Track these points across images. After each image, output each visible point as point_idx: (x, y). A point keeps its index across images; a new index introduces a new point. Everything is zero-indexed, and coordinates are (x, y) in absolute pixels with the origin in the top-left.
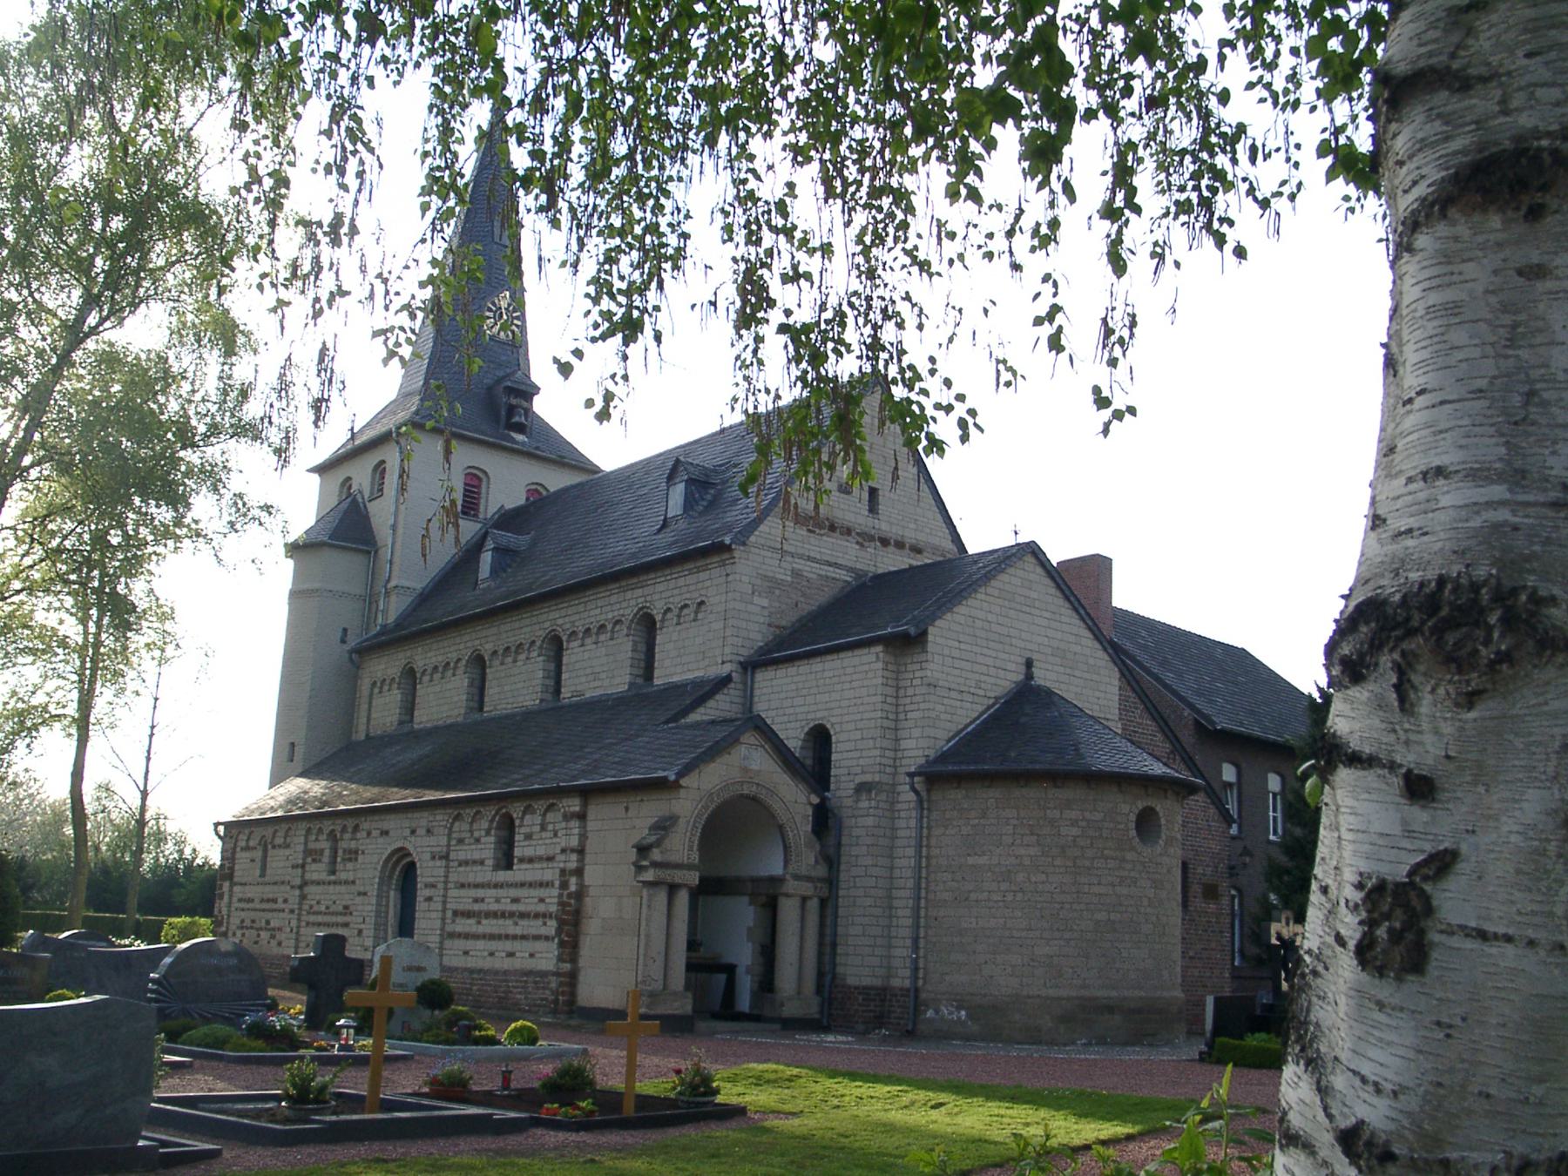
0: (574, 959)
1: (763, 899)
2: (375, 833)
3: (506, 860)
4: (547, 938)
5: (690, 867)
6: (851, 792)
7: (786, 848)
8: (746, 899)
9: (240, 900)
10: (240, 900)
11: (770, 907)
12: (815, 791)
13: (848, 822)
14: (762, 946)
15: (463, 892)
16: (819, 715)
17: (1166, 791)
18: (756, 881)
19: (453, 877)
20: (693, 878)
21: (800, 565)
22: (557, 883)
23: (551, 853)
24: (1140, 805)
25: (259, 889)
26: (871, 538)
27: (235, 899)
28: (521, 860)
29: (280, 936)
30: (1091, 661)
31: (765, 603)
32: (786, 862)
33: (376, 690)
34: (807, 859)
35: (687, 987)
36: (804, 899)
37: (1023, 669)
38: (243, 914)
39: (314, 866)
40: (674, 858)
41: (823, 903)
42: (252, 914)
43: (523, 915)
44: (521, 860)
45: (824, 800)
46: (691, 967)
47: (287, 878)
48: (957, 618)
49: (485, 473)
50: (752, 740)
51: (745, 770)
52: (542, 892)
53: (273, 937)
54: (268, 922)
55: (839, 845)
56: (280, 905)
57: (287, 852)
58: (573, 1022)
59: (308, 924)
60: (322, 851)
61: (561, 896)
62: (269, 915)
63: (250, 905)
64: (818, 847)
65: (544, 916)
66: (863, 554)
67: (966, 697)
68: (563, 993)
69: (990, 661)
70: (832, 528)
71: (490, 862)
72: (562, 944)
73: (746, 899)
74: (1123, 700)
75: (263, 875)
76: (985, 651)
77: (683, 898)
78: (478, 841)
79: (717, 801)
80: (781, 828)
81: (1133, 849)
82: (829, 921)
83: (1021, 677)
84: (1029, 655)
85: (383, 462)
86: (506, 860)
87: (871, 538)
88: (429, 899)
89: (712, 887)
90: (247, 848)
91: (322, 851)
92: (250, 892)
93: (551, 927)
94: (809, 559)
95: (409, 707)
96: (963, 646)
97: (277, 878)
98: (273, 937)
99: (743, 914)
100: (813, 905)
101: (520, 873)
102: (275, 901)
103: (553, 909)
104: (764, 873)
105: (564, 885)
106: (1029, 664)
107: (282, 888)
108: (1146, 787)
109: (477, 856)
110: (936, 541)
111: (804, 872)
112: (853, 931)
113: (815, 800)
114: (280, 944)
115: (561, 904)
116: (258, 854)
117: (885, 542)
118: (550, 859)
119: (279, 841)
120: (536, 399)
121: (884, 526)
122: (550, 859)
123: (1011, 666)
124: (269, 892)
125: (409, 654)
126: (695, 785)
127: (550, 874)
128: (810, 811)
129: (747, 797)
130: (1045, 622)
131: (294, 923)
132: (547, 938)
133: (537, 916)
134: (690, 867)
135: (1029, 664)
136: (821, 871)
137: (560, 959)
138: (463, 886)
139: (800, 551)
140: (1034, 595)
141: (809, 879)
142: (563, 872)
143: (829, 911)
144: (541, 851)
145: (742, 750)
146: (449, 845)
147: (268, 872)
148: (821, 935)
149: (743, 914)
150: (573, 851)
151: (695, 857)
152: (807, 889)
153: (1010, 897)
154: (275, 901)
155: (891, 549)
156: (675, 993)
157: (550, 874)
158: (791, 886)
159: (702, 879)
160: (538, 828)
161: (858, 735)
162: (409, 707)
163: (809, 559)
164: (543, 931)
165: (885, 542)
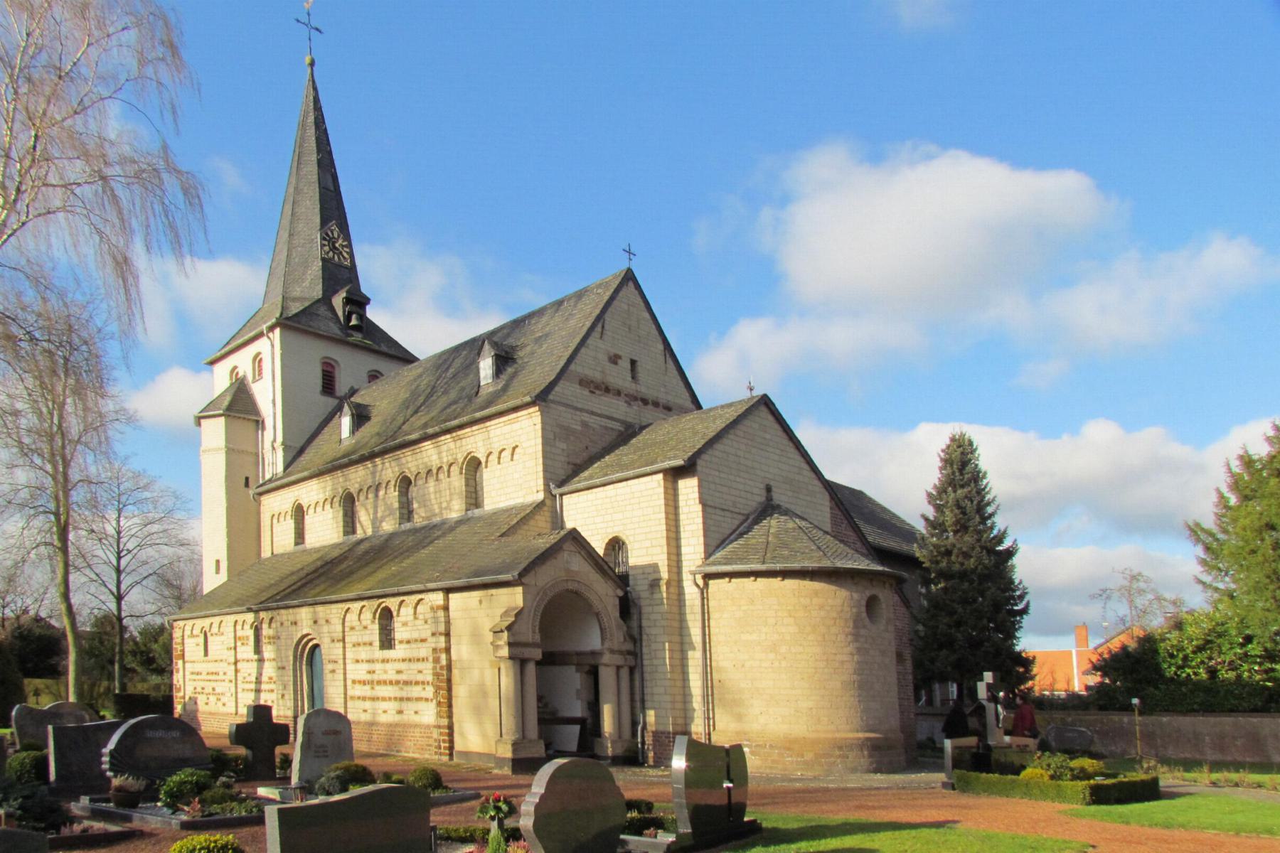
0: (450, 716)
1: (587, 668)
2: (221, 673)
3: (387, 641)
4: (427, 700)
5: (534, 645)
6: (646, 587)
7: (601, 629)
8: (573, 668)
9: (192, 673)
10: (192, 673)
11: (594, 673)
12: (620, 587)
13: (645, 610)
14: (589, 703)
15: (359, 666)
16: (616, 529)
17: (884, 583)
18: (579, 654)
19: (349, 655)
20: (537, 654)
21: (592, 420)
22: (431, 659)
23: (423, 636)
24: (868, 593)
25: (204, 665)
26: (636, 399)
27: (187, 673)
28: (401, 642)
29: (224, 699)
30: (810, 487)
31: (564, 446)
32: (603, 639)
33: (275, 521)
34: (618, 638)
35: (540, 737)
36: (618, 668)
37: (764, 493)
38: (195, 684)
39: (244, 648)
40: (523, 639)
41: (632, 670)
42: (202, 684)
43: (406, 683)
44: (401, 642)
45: (626, 593)
46: (541, 721)
47: (224, 657)
48: (717, 453)
49: (336, 361)
50: (573, 548)
51: (568, 571)
52: (420, 666)
53: (219, 699)
54: (214, 689)
55: (640, 627)
56: (221, 677)
57: (222, 638)
58: (473, 774)
59: (243, 690)
60: (248, 638)
61: (434, 668)
62: (213, 684)
63: (199, 677)
64: (625, 628)
65: (423, 683)
66: (628, 410)
67: (728, 514)
68: (444, 741)
69: (741, 487)
70: (607, 390)
71: (377, 643)
72: (439, 704)
73: (573, 668)
74: (833, 517)
75: (206, 654)
76: (738, 479)
77: (531, 669)
78: (365, 628)
79: (550, 594)
80: (597, 615)
81: (864, 627)
82: (637, 683)
83: (763, 499)
84: (767, 482)
85: (259, 354)
86: (387, 641)
87: (636, 399)
88: (333, 671)
89: (550, 660)
90: (192, 636)
91: (248, 638)
92: (198, 667)
93: (429, 692)
94: (592, 413)
95: (300, 536)
96: (722, 475)
97: (216, 658)
98: (219, 699)
99: (572, 679)
100: (625, 673)
101: (399, 651)
102: (217, 674)
103: (430, 678)
104: (589, 648)
105: (437, 660)
106: (769, 489)
107: (222, 664)
108: (871, 580)
109: (367, 639)
110: (680, 401)
111: (616, 647)
112: (656, 690)
113: (620, 593)
114: (224, 705)
115: (436, 675)
116: (201, 640)
117: (645, 402)
118: (423, 641)
119: (215, 629)
120: (368, 308)
121: (643, 390)
122: (423, 641)
123: (756, 491)
124: (212, 667)
125: (296, 493)
126: (533, 582)
127: (425, 651)
128: (617, 602)
129: (571, 591)
130: (776, 458)
131: (233, 690)
132: (427, 700)
133: (417, 683)
134: (534, 645)
135: (769, 489)
136: (629, 646)
137: (439, 715)
138: (357, 661)
139: (586, 407)
140: (768, 436)
141: (621, 652)
142: (435, 650)
143: (637, 677)
144: (415, 635)
145: (566, 555)
146: (344, 632)
147: (210, 652)
148: (632, 694)
149: (572, 680)
150: (441, 634)
151: (538, 638)
152: (618, 660)
153: (777, 664)
154: (217, 674)
155: (650, 407)
156: (530, 741)
157: (425, 651)
158: (607, 658)
159: (544, 654)
160: (411, 618)
161: (648, 544)
162: (300, 536)
163: (592, 413)
164: (423, 694)
165: (645, 402)
